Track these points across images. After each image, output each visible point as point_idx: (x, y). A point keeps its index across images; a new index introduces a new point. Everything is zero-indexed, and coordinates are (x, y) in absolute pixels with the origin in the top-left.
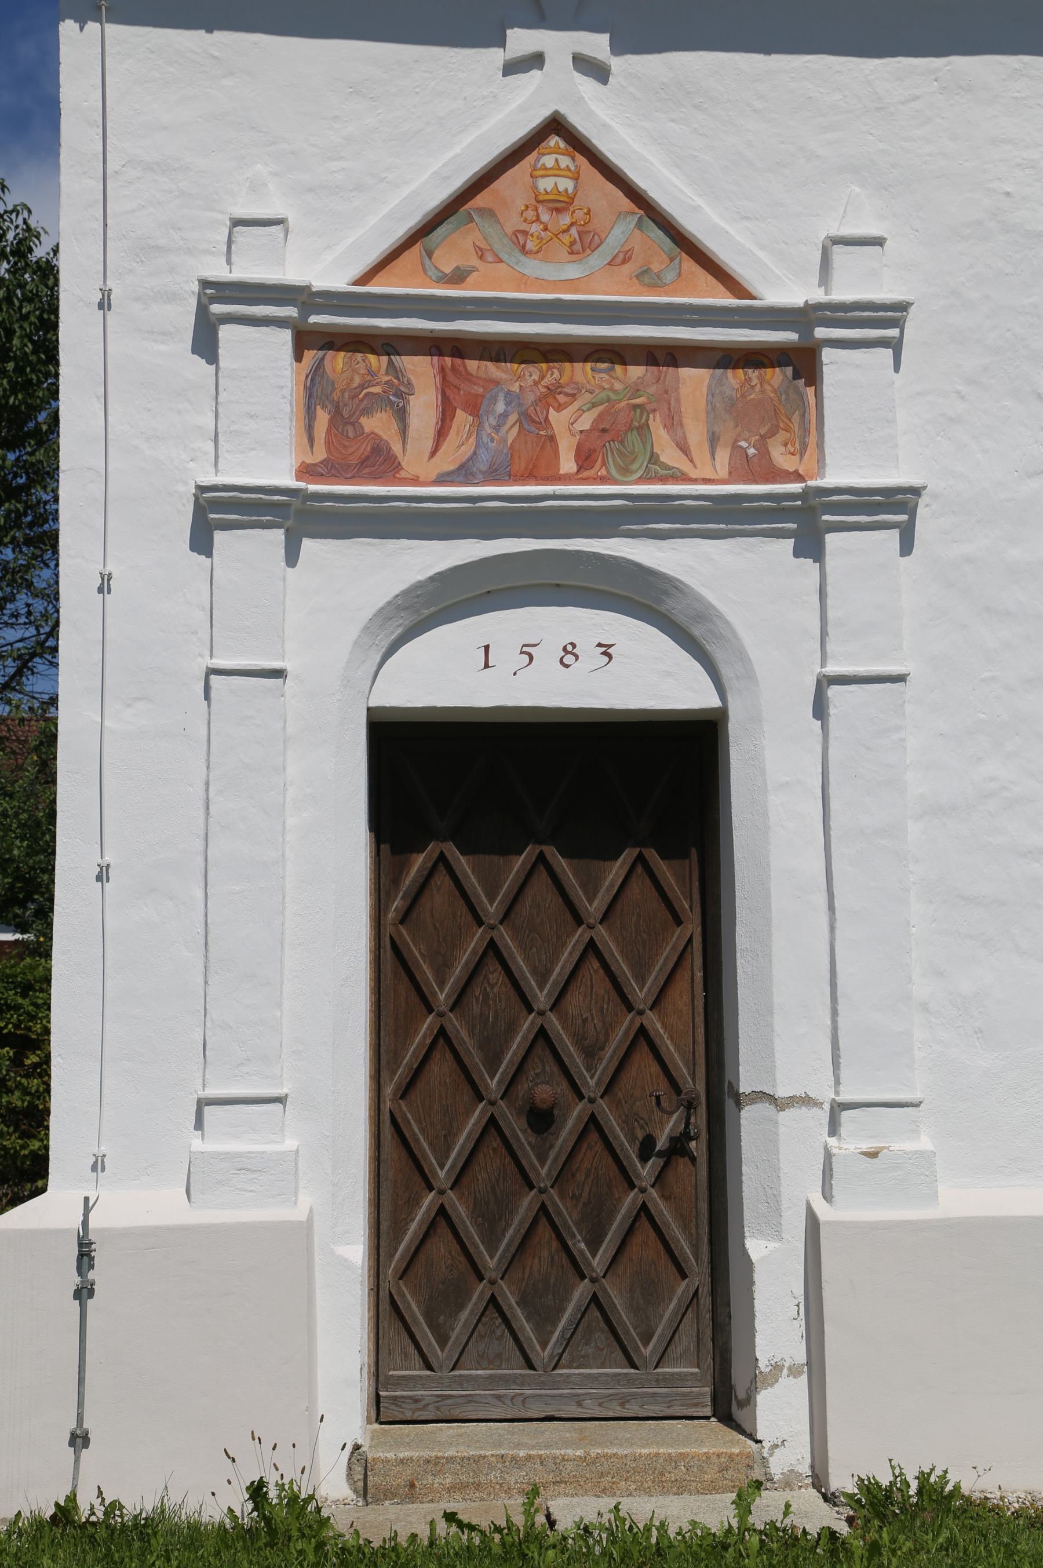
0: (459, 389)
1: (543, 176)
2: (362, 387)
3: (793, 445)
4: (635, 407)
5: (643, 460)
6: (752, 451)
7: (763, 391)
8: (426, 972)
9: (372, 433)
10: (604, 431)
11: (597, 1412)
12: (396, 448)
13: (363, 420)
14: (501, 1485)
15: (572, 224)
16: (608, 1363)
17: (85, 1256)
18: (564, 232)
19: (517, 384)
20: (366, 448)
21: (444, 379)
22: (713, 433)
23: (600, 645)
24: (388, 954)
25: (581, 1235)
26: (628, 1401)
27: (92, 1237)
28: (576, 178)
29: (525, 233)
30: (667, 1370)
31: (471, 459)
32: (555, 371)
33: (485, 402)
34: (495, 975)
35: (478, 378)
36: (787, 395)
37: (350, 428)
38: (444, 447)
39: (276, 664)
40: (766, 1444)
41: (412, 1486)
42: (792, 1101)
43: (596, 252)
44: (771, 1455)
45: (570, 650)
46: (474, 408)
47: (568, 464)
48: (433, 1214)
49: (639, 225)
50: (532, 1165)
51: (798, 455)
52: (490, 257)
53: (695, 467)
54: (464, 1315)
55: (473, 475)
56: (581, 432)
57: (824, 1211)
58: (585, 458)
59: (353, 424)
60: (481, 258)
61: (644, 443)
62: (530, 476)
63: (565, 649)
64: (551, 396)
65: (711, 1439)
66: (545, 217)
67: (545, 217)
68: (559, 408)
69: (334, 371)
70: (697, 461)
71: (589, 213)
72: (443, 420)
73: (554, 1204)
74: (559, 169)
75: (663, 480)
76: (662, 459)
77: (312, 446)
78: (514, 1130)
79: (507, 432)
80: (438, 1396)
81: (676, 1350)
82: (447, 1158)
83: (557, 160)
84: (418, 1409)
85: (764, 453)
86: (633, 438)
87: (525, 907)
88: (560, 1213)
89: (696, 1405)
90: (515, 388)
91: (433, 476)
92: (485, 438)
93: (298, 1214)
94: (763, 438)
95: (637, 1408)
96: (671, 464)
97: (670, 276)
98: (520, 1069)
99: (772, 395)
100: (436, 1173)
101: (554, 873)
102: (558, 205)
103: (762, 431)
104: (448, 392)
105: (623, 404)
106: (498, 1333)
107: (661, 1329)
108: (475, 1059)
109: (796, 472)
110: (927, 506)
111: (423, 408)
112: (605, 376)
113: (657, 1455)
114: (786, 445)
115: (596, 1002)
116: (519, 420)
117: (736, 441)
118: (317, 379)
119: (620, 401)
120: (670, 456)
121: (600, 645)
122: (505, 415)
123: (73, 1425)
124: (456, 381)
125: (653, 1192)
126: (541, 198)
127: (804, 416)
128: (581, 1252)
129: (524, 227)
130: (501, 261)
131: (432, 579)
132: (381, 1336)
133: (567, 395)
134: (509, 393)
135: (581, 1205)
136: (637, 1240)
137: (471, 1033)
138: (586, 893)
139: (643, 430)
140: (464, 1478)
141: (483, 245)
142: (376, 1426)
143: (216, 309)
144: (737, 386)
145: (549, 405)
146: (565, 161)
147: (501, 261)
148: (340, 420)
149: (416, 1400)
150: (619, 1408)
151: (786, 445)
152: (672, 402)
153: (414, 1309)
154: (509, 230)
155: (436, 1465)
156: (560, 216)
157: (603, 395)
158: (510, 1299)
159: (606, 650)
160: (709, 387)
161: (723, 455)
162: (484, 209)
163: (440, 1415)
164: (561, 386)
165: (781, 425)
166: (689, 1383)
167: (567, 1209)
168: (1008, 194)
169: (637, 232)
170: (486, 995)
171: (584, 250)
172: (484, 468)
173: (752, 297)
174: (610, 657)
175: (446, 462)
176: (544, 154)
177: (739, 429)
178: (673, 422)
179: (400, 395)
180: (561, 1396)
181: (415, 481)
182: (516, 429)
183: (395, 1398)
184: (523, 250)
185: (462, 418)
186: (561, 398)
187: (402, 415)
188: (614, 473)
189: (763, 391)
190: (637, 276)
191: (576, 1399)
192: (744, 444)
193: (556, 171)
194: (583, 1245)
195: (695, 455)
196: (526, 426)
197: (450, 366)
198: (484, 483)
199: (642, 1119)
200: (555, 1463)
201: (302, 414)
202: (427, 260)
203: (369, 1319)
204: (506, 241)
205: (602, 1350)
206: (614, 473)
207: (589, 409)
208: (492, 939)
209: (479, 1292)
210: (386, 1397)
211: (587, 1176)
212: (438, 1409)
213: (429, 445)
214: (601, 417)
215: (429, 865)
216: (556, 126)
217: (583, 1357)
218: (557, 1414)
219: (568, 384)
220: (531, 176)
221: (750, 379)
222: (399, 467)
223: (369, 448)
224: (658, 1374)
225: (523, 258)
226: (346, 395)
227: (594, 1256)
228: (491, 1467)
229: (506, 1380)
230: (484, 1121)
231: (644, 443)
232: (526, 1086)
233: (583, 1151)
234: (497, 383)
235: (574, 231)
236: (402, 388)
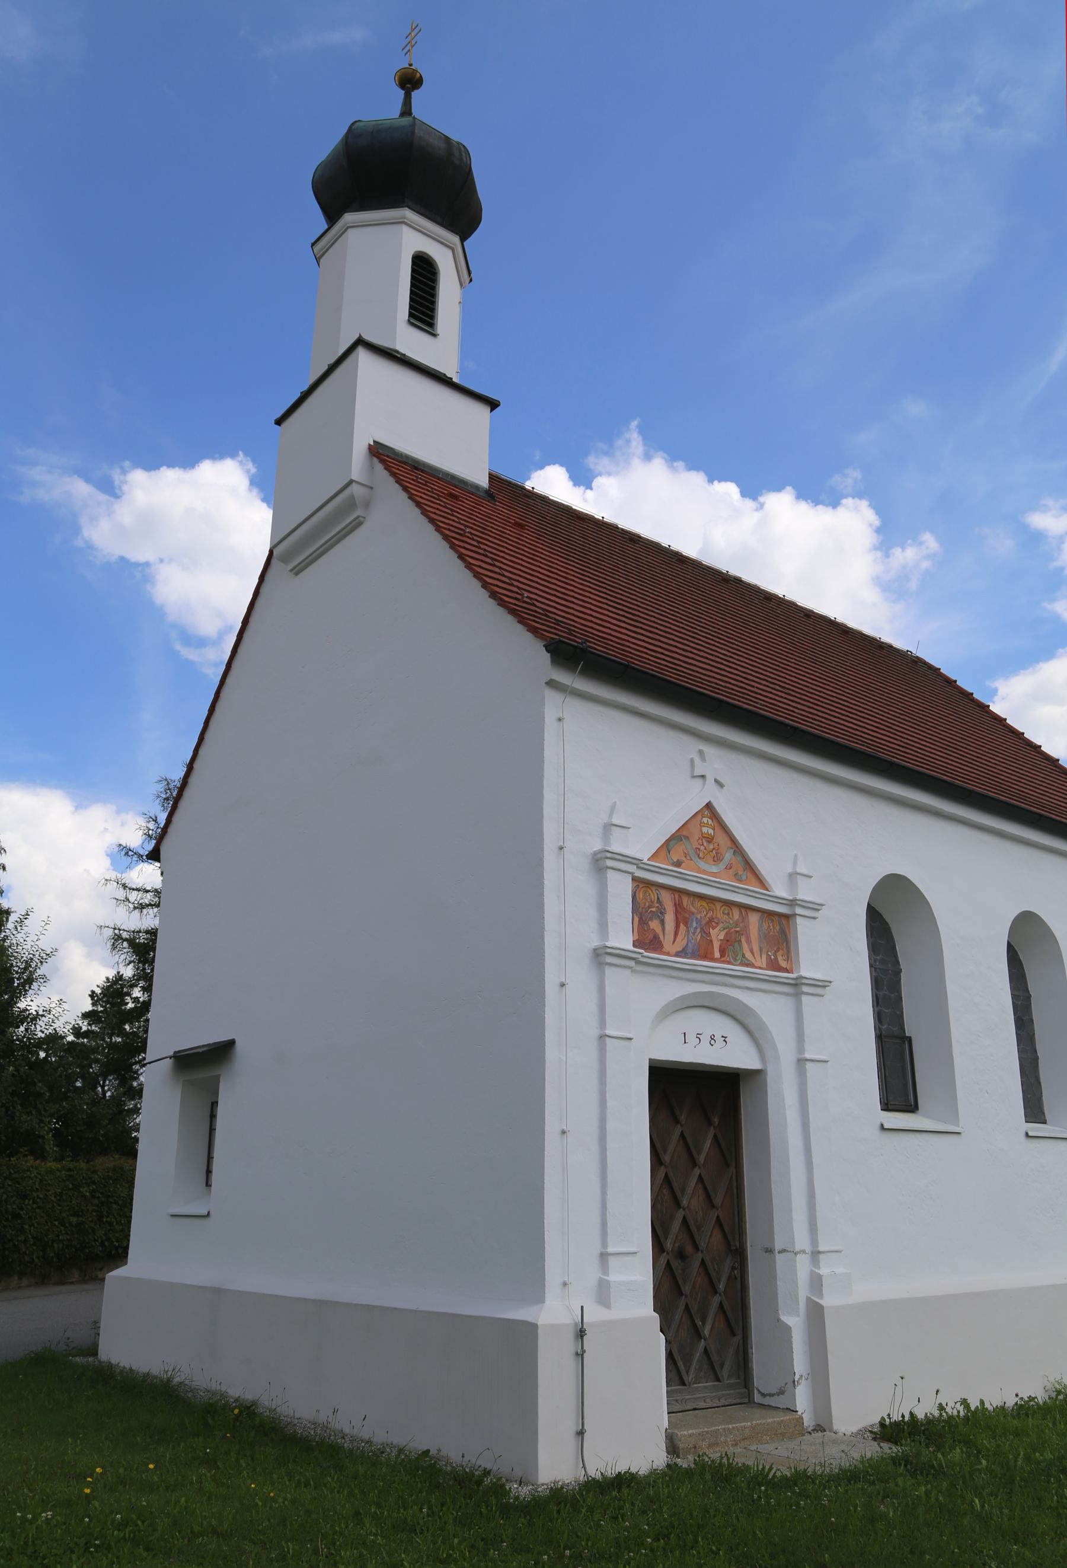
5: (740, 957)
12: (662, 937)
17: (581, 1333)
20: (651, 936)
39: (629, 1035)
42: (799, 1252)
68: (713, 928)
86: (736, 945)
97: (744, 877)
111: (670, 918)
120: (748, 955)
122: (696, 928)
146: (710, 822)
178: (749, 941)
179: (661, 913)
181: (668, 954)
187: (662, 922)
193: (707, 825)
234: (693, 913)
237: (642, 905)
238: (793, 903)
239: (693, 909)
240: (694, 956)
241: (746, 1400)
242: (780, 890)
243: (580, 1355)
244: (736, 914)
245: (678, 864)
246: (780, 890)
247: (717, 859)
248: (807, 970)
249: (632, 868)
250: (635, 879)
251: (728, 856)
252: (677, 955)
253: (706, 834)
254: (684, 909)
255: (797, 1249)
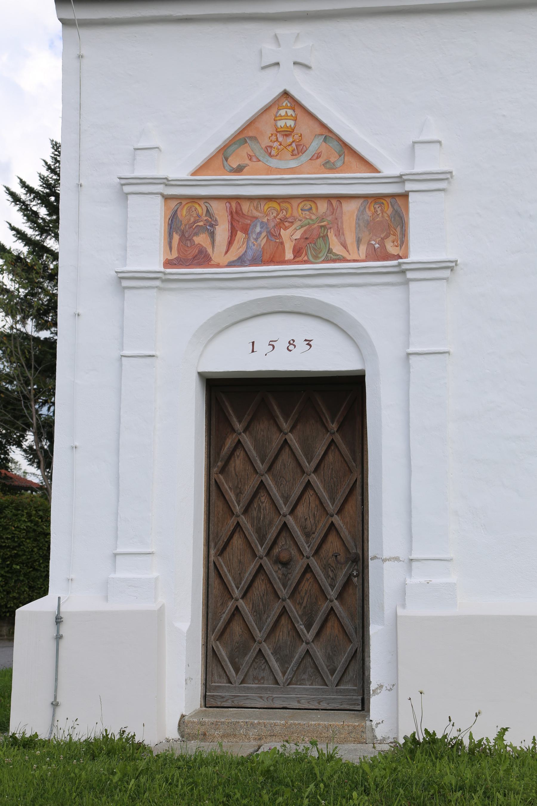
0: (239, 222)
1: (280, 120)
2: (195, 222)
3: (397, 242)
4: (321, 226)
5: (324, 253)
6: (377, 246)
7: (383, 217)
8: (231, 496)
9: (199, 244)
10: (306, 239)
11: (306, 706)
12: (210, 250)
13: (195, 238)
14: (245, 736)
15: (293, 142)
16: (314, 684)
17: (58, 620)
18: (289, 145)
19: (266, 218)
21: (232, 217)
22: (359, 238)
23: (306, 340)
24: (213, 488)
25: (302, 620)
26: (322, 701)
27: (62, 615)
28: (295, 120)
29: (271, 147)
30: (342, 687)
31: (244, 254)
32: (284, 211)
33: (251, 227)
34: (264, 498)
35: (248, 216)
36: (395, 218)
37: (188, 242)
38: (232, 249)
40: (374, 723)
41: (205, 734)
43: (304, 154)
44: (376, 727)
45: (292, 343)
46: (246, 230)
47: (289, 255)
48: (233, 610)
49: (325, 140)
50: (279, 588)
51: (399, 247)
52: (254, 159)
53: (350, 254)
54: (247, 658)
55: (245, 262)
56: (296, 239)
57: (401, 612)
58: (297, 252)
59: (190, 240)
60: (250, 160)
61: (325, 244)
62: (272, 261)
63: (289, 342)
64: (282, 223)
65: (349, 721)
66: (280, 139)
67: (280, 139)
68: (286, 228)
69: (182, 215)
70: (351, 252)
71: (301, 136)
72: (231, 236)
73: (289, 606)
74: (288, 116)
75: (334, 261)
76: (334, 251)
77: (171, 251)
78: (271, 571)
79: (261, 241)
80: (233, 696)
81: (347, 678)
82: (240, 584)
83: (286, 112)
84: (224, 702)
85: (383, 246)
86: (320, 242)
87: (278, 465)
88: (292, 611)
89: (354, 704)
90: (265, 220)
91: (226, 263)
92: (250, 244)
93: (154, 606)
94: (383, 239)
95: (326, 705)
96: (338, 253)
97: (339, 164)
98: (275, 543)
99: (387, 218)
100: (235, 591)
101: (289, 449)
102: (287, 133)
103: (382, 236)
104: (234, 223)
105: (316, 225)
106: (263, 667)
107: (340, 668)
108: (254, 538)
109: (398, 255)
110: (462, 269)
111: (222, 232)
112: (307, 213)
113: (319, 724)
114: (393, 242)
115: (311, 511)
116: (267, 235)
117: (370, 241)
118: (174, 220)
119: (314, 224)
120: (337, 249)
121: (306, 340)
122: (260, 233)
123: (53, 700)
124: (238, 218)
125: (336, 602)
126: (279, 130)
127: (402, 228)
128: (302, 630)
129: (271, 144)
130: (260, 161)
131: (225, 311)
132: (208, 667)
133: (289, 222)
134: (262, 222)
135: (302, 607)
136: (329, 624)
137: (252, 526)
138: (307, 459)
139: (325, 238)
140: (229, 731)
141: (252, 154)
142: (205, 709)
143: (127, 189)
144: (370, 215)
145: (281, 227)
146: (290, 112)
147: (260, 161)
148: (185, 238)
149: (223, 697)
150: (317, 704)
151: (393, 242)
152: (339, 224)
153: (223, 653)
154: (264, 146)
155: (216, 725)
156: (287, 138)
157: (306, 222)
158: (268, 651)
159: (309, 343)
160: (357, 216)
161: (363, 248)
162: (252, 137)
163: (234, 705)
164: (287, 218)
165: (392, 232)
166: (352, 694)
167: (296, 609)
168: (504, 116)
169: (324, 144)
170: (260, 507)
171: (298, 154)
172: (249, 258)
173: (377, 171)
174: (310, 346)
175: (233, 255)
176: (280, 110)
177: (371, 235)
178: (339, 233)
180: (291, 698)
181: (218, 266)
182: (265, 240)
183: (213, 696)
184: (270, 155)
185: (240, 235)
186: (287, 224)
187: (212, 235)
188: (311, 258)
189: (383, 217)
190: (323, 165)
191: (298, 699)
192: (373, 242)
194: (302, 627)
195: (350, 248)
196: (270, 238)
197: (235, 211)
198: (250, 265)
199: (332, 567)
200: (271, 727)
201: (167, 235)
202: (225, 163)
203: (202, 658)
204: (262, 151)
205: (311, 677)
206: (311, 258)
207: (299, 229)
208: (262, 481)
209: (255, 647)
210: (209, 696)
211: (306, 594)
212: (233, 702)
213: (224, 248)
214: (305, 232)
215: (233, 445)
216: (286, 94)
217: (303, 680)
218: (288, 706)
219: (290, 217)
220: (274, 120)
221: (377, 211)
222: (210, 259)
223: (197, 251)
224: (337, 689)
225: (270, 159)
226: (187, 227)
227: (308, 633)
228: (241, 727)
229: (266, 689)
230: (257, 567)
231: (325, 244)
232: (277, 550)
233: (304, 582)
234: (256, 218)
235: (294, 145)
236: (213, 222)
237: (184, 222)
238: (401, 179)
239: (256, 214)
240: (255, 262)
241: (359, 708)
242: (391, 167)
243: (59, 638)
244: (323, 207)
245: (239, 170)
246: (391, 167)
247: (299, 150)
248: (419, 251)
249: (160, 188)
250: (167, 198)
251: (315, 145)
252: (230, 265)
253: (286, 126)
254: (243, 216)
255: (386, 555)
